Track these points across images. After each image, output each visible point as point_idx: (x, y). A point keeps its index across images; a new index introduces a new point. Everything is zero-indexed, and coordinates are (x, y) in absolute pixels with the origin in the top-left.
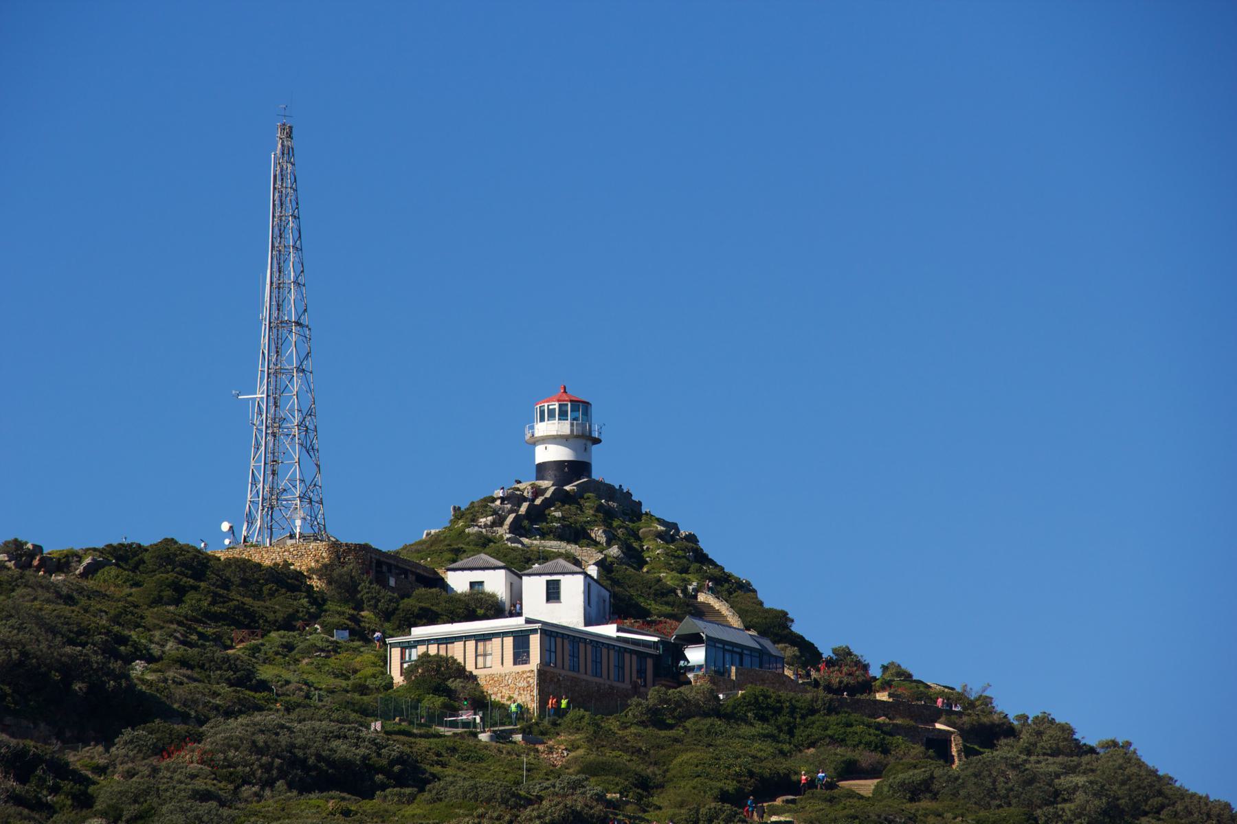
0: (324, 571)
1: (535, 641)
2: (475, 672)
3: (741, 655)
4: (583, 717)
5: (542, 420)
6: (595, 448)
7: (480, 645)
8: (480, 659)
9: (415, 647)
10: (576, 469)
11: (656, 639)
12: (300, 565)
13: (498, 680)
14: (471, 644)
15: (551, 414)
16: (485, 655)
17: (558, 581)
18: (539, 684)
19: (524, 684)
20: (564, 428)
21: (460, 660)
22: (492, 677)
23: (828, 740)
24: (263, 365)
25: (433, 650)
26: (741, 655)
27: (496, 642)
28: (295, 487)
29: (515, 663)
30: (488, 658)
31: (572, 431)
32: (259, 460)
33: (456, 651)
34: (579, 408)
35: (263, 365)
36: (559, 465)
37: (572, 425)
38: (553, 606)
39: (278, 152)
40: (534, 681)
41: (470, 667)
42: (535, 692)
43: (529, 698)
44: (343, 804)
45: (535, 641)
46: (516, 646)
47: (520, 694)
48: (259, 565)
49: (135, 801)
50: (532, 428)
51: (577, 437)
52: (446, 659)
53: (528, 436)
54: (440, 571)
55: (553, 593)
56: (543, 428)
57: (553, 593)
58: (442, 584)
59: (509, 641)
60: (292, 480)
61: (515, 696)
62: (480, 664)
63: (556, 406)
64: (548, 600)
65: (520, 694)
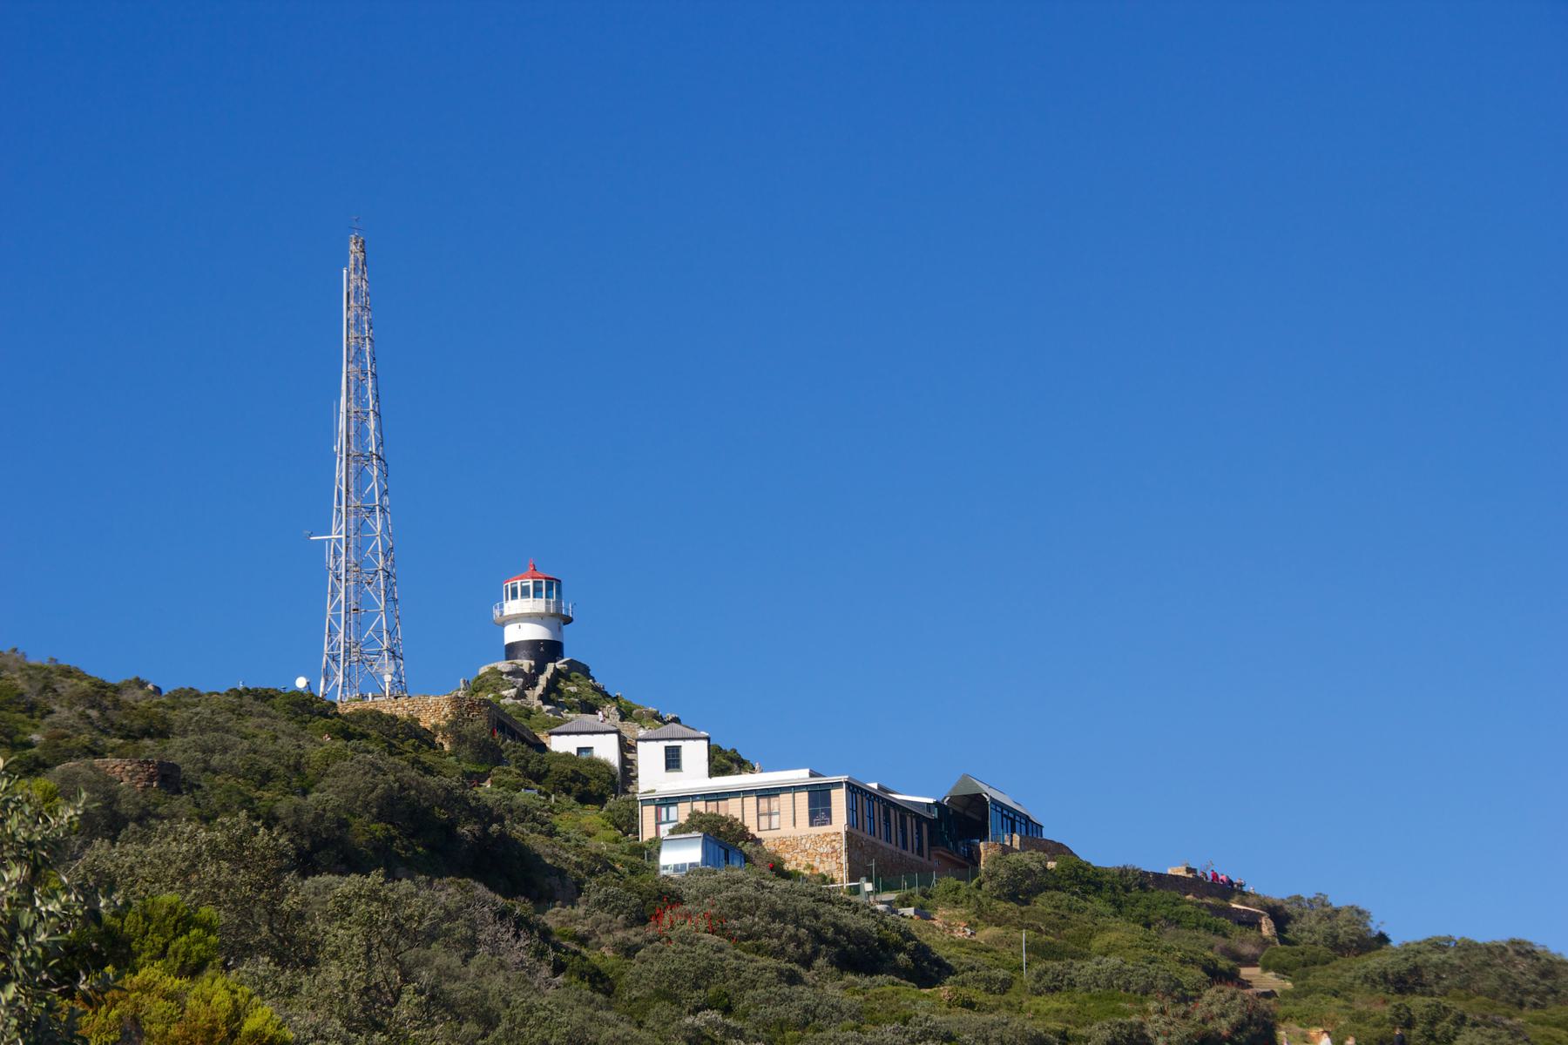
0: (454, 728)
1: (839, 799)
2: (758, 835)
3: (1013, 821)
4: (958, 888)
5: (514, 596)
6: (565, 627)
7: (764, 803)
8: (764, 819)
9: (675, 804)
10: (547, 651)
11: (931, 801)
12: (427, 721)
13: (794, 845)
14: (751, 801)
15: (525, 592)
16: (770, 814)
17: (678, 749)
18: (848, 849)
19: (828, 849)
20: (537, 605)
21: (738, 815)
22: (783, 841)
23: (1163, 922)
24: (340, 503)
25: (700, 806)
26: (1013, 821)
27: (785, 798)
28: (381, 637)
29: (811, 824)
30: (775, 818)
31: (547, 608)
32: (338, 608)
33: (732, 808)
34: (551, 586)
35: (340, 503)
36: (534, 645)
37: (548, 603)
38: (673, 775)
39: (352, 267)
40: (842, 846)
41: (753, 830)
42: (844, 859)
43: (834, 866)
44: (963, 991)
45: (839, 799)
46: (812, 803)
47: (822, 862)
48: (394, 717)
49: (697, 987)
50: (502, 606)
51: (553, 615)
52: (723, 820)
53: (497, 613)
54: (542, 736)
55: (673, 760)
56: (513, 607)
57: (673, 760)
58: (542, 748)
59: (803, 797)
60: (378, 631)
61: (816, 864)
62: (764, 825)
63: (531, 583)
64: (668, 767)
65: (822, 862)
